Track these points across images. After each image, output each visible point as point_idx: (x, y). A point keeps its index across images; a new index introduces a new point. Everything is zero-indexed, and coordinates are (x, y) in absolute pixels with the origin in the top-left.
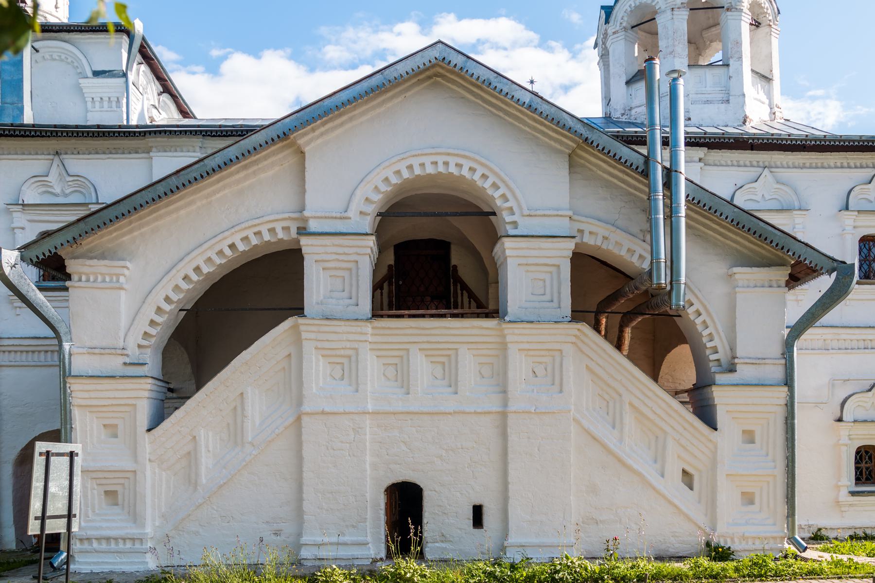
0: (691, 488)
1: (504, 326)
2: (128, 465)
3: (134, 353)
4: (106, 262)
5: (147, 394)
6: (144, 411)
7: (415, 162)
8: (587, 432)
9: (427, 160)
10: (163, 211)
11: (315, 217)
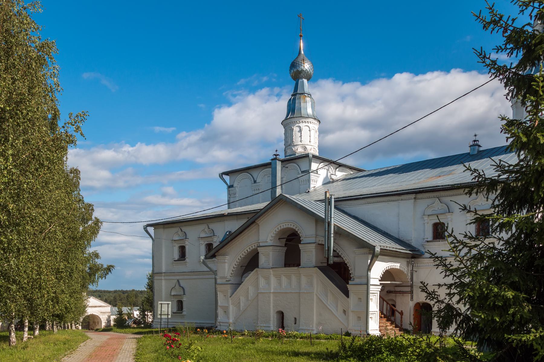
0: (345, 314)
1: (299, 269)
2: (227, 305)
3: (229, 277)
4: (222, 257)
5: (314, 247)
6: (230, 292)
7: (281, 225)
8: (319, 298)
9: (284, 224)
10: (233, 243)
11: (441, 214)
